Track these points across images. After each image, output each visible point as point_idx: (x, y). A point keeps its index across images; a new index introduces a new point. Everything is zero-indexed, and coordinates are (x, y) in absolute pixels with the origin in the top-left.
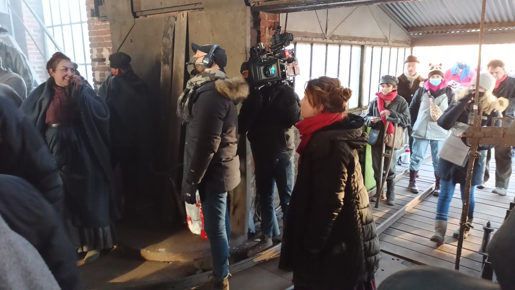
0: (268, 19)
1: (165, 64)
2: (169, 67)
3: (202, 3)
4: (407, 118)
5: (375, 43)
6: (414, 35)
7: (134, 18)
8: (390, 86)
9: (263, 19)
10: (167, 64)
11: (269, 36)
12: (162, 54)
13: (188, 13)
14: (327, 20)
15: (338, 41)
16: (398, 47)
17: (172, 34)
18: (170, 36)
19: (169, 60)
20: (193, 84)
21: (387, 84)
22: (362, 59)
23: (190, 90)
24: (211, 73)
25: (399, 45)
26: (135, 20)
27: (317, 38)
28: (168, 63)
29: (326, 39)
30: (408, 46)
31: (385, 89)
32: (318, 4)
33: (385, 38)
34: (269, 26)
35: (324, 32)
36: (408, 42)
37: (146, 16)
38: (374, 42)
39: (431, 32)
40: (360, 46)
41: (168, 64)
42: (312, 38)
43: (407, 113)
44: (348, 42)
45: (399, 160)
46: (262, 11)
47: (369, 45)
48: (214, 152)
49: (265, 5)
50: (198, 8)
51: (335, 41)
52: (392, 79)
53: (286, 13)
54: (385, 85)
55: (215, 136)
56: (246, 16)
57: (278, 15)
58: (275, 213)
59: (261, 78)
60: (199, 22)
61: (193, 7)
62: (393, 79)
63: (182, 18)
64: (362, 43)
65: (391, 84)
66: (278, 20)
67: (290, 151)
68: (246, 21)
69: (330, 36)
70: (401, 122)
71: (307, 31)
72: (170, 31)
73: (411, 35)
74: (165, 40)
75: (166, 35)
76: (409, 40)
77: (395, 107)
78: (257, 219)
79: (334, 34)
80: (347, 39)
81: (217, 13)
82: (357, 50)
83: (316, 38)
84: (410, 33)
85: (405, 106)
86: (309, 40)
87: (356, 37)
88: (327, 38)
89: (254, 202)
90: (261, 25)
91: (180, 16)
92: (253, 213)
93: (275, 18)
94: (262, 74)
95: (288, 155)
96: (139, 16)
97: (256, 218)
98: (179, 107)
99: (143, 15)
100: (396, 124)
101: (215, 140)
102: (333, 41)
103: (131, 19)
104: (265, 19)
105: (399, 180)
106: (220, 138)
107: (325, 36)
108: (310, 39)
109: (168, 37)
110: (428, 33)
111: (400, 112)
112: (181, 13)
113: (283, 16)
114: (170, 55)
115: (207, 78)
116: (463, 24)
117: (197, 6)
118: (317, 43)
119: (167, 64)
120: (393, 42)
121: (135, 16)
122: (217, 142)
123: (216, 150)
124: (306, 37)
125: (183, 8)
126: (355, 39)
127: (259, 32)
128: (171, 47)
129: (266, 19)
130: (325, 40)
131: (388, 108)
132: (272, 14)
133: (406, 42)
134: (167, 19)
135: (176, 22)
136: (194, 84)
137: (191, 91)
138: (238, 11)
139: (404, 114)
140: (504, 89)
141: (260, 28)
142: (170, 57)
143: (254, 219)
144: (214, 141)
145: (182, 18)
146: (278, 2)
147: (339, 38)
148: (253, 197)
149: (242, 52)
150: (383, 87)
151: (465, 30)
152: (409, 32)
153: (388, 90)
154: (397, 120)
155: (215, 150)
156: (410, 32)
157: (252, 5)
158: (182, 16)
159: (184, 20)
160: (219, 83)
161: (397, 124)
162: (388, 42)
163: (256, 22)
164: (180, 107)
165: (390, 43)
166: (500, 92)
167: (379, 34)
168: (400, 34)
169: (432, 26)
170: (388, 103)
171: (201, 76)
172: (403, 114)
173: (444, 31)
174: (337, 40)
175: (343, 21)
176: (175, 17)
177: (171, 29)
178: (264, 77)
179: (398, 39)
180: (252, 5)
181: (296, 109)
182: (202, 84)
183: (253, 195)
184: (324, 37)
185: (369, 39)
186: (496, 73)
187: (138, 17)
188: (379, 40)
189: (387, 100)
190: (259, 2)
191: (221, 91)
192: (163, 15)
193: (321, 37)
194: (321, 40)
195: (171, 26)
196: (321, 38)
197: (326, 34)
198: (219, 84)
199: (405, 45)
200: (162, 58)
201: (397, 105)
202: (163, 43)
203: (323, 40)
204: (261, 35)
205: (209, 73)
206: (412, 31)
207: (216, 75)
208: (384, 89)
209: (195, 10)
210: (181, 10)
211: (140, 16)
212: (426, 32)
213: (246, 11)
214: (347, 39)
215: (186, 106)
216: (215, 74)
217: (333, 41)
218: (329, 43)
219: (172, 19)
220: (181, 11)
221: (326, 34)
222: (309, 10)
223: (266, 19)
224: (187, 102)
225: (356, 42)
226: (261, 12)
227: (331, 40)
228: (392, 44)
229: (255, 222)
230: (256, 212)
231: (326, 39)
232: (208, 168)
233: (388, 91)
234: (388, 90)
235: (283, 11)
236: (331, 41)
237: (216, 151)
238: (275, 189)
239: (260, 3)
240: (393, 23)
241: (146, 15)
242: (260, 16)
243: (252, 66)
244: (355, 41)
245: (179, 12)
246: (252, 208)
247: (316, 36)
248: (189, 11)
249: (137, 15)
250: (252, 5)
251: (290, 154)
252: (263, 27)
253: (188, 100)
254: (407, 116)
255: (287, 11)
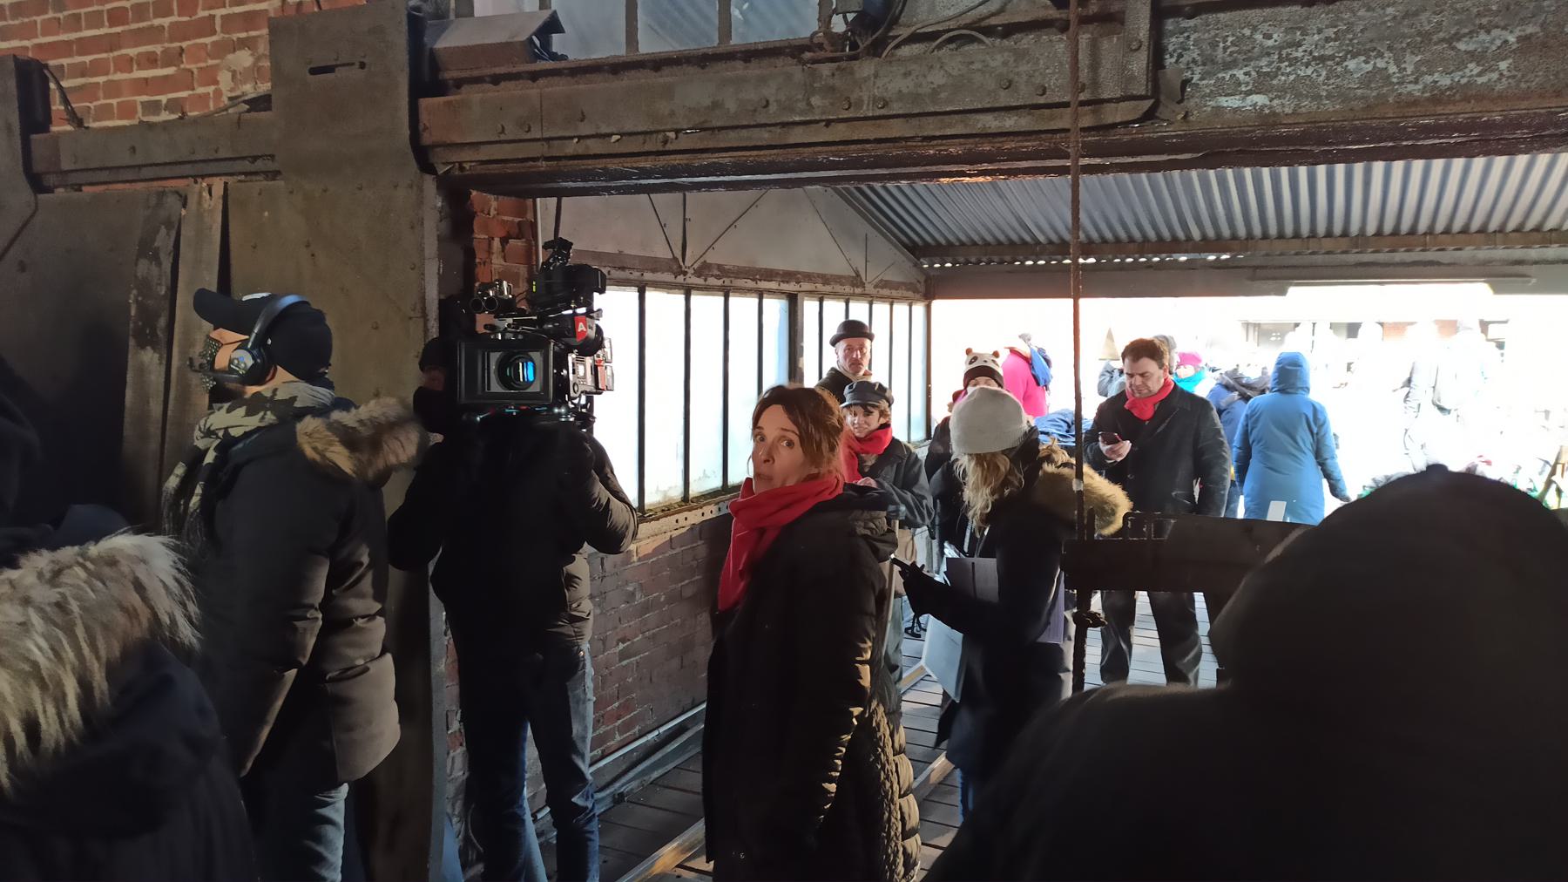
0: (498, 214)
1: (142, 345)
2: (157, 355)
3: (276, 158)
4: (924, 502)
5: (828, 288)
6: (931, 266)
7: (33, 194)
8: (872, 412)
9: (482, 212)
10: (149, 348)
11: (504, 263)
12: (133, 312)
13: (229, 185)
14: (685, 220)
15: (720, 282)
16: (892, 301)
17: (171, 247)
18: (162, 256)
19: (159, 333)
20: (217, 435)
21: (864, 406)
22: (792, 334)
23: (207, 450)
24: (277, 398)
25: (894, 293)
26: (36, 198)
27: (657, 272)
28: (155, 346)
29: (685, 273)
30: (917, 296)
31: (859, 420)
32: (647, 179)
33: (854, 275)
34: (503, 235)
35: (678, 254)
36: (918, 285)
37: (78, 187)
38: (824, 284)
39: (973, 260)
40: (784, 296)
41: (153, 348)
42: (642, 271)
43: (922, 488)
44: (751, 284)
45: (913, 623)
46: (478, 190)
47: (811, 294)
48: (297, 665)
49: (483, 172)
50: (263, 172)
51: (712, 281)
52: (875, 393)
53: (555, 199)
54: (860, 410)
55: (298, 613)
56: (422, 202)
57: (530, 202)
58: (531, 828)
59: (489, 389)
60: (266, 214)
61: (247, 166)
62: (879, 392)
63: (208, 197)
64: (791, 287)
65: (874, 406)
66: (530, 216)
67: (578, 624)
68: (423, 219)
69: (696, 266)
70: (909, 515)
71: (627, 252)
72: (163, 240)
73: (923, 268)
74: (143, 267)
75: (147, 250)
76: (918, 281)
77: (889, 472)
78: (472, 856)
79: (708, 262)
80: (746, 276)
81: (325, 191)
82: (775, 308)
83: (654, 271)
84: (921, 263)
85: (916, 469)
86: (631, 277)
87: (772, 270)
88: (686, 272)
89: (461, 796)
90: (476, 231)
91: (200, 193)
92: (458, 837)
93: (521, 212)
94: (493, 377)
95: (570, 636)
96: (51, 185)
97: (470, 853)
98: (168, 517)
99: (67, 185)
100: (895, 523)
101: (298, 624)
102: (705, 280)
103: (25, 193)
104: (489, 214)
105: (915, 685)
106: (320, 616)
107: (681, 267)
108: (636, 274)
109: (156, 258)
110: (968, 262)
111: (902, 488)
112: (204, 184)
113: (545, 207)
114: (160, 316)
115: (263, 418)
116: (1051, 242)
117: (259, 165)
118: (659, 285)
119: (149, 348)
120: (876, 287)
121: (38, 184)
122: (305, 629)
123: (304, 656)
124: (623, 268)
125: (212, 168)
126: (769, 275)
127: (470, 253)
128: (166, 292)
129: (491, 214)
130: (680, 279)
131: (873, 472)
132: (508, 201)
133: (910, 287)
134: (153, 201)
135: (183, 212)
136: (221, 434)
137: (210, 458)
138: (396, 187)
139: (915, 490)
140: (1167, 421)
141: (472, 240)
142: (162, 322)
143: (463, 853)
144: (295, 629)
145: (208, 197)
146: (523, 168)
147: (723, 272)
148: (460, 780)
149: (412, 313)
150: (855, 415)
151: (1059, 257)
152: (919, 260)
153: (869, 425)
154: (897, 511)
155: (301, 659)
156: (922, 260)
157: (440, 172)
158: (206, 194)
159: (214, 204)
160: (309, 430)
161: (897, 522)
162: (863, 285)
163: (460, 222)
164: (171, 515)
165: (869, 289)
166: (1159, 431)
167: (838, 265)
168: (897, 266)
169: (974, 244)
170: (871, 461)
171: (242, 411)
172: (913, 493)
173: (1008, 258)
174: (718, 277)
175: (754, 206)
176: (181, 196)
177: (168, 234)
178: (496, 387)
179: (890, 276)
180: (440, 172)
181: (594, 497)
182: (247, 435)
183: (461, 773)
184: (679, 270)
185: (809, 277)
186: (1142, 375)
187: (50, 190)
188: (838, 279)
189: (867, 453)
190: (465, 165)
191: (317, 458)
192: (140, 186)
193: (670, 270)
194: (669, 277)
195: (168, 224)
196: (668, 271)
197: (684, 261)
198: (310, 435)
199: (910, 294)
200: (131, 325)
201: (895, 466)
202: (136, 276)
203: (676, 277)
204: (477, 260)
205: (272, 397)
206: (924, 256)
207: (298, 404)
208: (856, 422)
209: (254, 178)
210: (205, 173)
211: (57, 187)
212: (962, 259)
213: (421, 190)
214: (746, 276)
215: (192, 513)
216: (294, 399)
217: (705, 280)
218: (694, 288)
219: (172, 201)
220: (203, 177)
221: (684, 261)
222: (622, 194)
223: (493, 212)
224: (195, 500)
225: (773, 285)
226: (474, 193)
227: (699, 277)
228: (874, 292)
229: (465, 866)
230: (470, 831)
231: (685, 275)
232: (274, 724)
233: (866, 426)
234: (869, 425)
235: (547, 194)
236: (700, 281)
237: (305, 661)
238: (531, 753)
239: (467, 166)
240: (872, 233)
241: (81, 185)
242: (471, 204)
243: (463, 346)
244: (769, 281)
245: (196, 182)
246: (455, 820)
247: (654, 265)
248: (230, 180)
249: (45, 183)
250: (442, 170)
251: (580, 635)
252: (483, 236)
253: (198, 490)
254: (924, 498)
255: (560, 194)
